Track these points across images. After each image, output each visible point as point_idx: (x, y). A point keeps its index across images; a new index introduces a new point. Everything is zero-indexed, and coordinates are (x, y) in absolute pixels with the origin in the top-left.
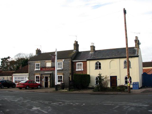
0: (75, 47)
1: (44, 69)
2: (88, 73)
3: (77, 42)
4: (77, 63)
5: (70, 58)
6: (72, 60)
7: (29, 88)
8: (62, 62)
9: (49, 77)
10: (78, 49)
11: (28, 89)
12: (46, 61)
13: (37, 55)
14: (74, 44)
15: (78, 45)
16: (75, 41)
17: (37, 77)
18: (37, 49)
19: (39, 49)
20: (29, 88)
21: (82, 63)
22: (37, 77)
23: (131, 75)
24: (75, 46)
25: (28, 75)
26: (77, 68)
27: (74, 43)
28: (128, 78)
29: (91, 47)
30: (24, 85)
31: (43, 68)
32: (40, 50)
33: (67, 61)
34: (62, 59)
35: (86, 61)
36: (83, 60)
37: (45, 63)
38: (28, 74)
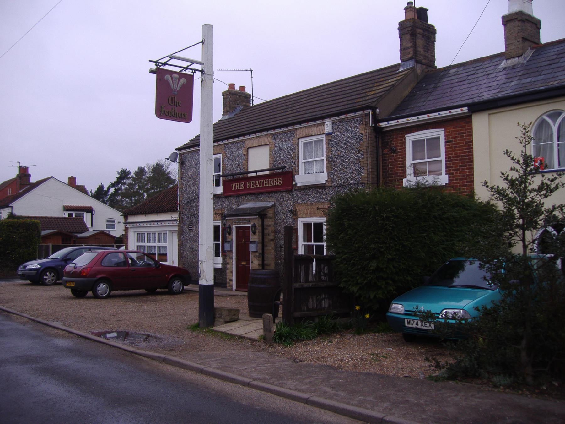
0: (409, 45)
1: (239, 186)
2: (29, 173)
3: (422, 13)
4: (409, 139)
5: (363, 109)
6: (376, 120)
7: (113, 293)
8: (324, 137)
9: (254, 233)
10: (432, 59)
11: (109, 297)
12: (250, 140)
13: (226, 117)
14: (402, 27)
15: (430, 32)
16: (410, 8)
17: (307, 226)
18: (226, 88)
19: (243, 88)
20: (113, 293)
21: (440, 133)
22: (307, 226)
23: (155, 60)
24: (408, 37)
25: (176, 223)
26: (410, 171)
27: (403, 18)
28: (515, 208)
29: (507, 20)
30: (536, 242)
31: (234, 181)
32: (248, 91)
33: (347, 131)
34: (322, 118)
35: (466, 120)
36: (434, 115)
37: (243, 151)
38: (176, 216)
